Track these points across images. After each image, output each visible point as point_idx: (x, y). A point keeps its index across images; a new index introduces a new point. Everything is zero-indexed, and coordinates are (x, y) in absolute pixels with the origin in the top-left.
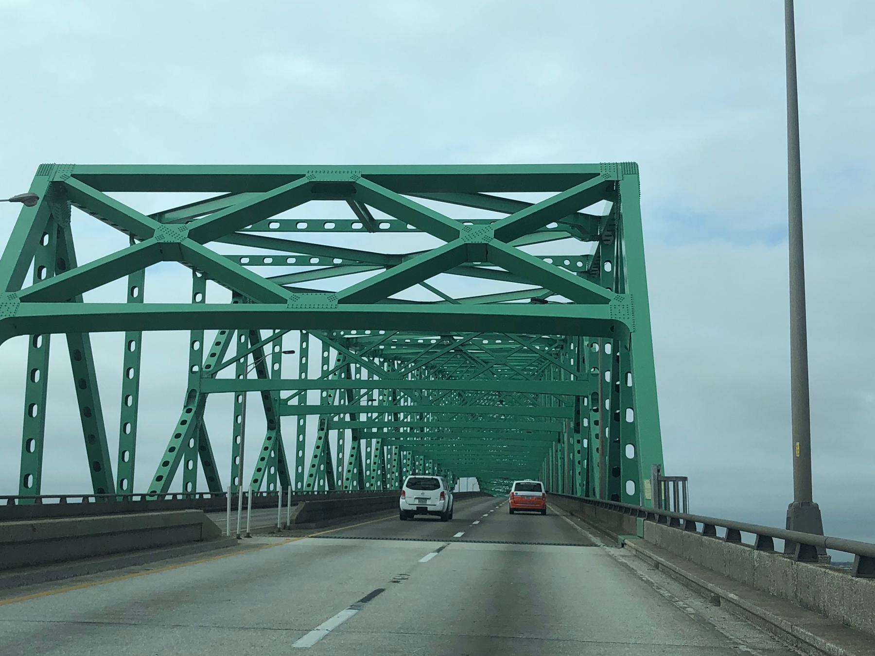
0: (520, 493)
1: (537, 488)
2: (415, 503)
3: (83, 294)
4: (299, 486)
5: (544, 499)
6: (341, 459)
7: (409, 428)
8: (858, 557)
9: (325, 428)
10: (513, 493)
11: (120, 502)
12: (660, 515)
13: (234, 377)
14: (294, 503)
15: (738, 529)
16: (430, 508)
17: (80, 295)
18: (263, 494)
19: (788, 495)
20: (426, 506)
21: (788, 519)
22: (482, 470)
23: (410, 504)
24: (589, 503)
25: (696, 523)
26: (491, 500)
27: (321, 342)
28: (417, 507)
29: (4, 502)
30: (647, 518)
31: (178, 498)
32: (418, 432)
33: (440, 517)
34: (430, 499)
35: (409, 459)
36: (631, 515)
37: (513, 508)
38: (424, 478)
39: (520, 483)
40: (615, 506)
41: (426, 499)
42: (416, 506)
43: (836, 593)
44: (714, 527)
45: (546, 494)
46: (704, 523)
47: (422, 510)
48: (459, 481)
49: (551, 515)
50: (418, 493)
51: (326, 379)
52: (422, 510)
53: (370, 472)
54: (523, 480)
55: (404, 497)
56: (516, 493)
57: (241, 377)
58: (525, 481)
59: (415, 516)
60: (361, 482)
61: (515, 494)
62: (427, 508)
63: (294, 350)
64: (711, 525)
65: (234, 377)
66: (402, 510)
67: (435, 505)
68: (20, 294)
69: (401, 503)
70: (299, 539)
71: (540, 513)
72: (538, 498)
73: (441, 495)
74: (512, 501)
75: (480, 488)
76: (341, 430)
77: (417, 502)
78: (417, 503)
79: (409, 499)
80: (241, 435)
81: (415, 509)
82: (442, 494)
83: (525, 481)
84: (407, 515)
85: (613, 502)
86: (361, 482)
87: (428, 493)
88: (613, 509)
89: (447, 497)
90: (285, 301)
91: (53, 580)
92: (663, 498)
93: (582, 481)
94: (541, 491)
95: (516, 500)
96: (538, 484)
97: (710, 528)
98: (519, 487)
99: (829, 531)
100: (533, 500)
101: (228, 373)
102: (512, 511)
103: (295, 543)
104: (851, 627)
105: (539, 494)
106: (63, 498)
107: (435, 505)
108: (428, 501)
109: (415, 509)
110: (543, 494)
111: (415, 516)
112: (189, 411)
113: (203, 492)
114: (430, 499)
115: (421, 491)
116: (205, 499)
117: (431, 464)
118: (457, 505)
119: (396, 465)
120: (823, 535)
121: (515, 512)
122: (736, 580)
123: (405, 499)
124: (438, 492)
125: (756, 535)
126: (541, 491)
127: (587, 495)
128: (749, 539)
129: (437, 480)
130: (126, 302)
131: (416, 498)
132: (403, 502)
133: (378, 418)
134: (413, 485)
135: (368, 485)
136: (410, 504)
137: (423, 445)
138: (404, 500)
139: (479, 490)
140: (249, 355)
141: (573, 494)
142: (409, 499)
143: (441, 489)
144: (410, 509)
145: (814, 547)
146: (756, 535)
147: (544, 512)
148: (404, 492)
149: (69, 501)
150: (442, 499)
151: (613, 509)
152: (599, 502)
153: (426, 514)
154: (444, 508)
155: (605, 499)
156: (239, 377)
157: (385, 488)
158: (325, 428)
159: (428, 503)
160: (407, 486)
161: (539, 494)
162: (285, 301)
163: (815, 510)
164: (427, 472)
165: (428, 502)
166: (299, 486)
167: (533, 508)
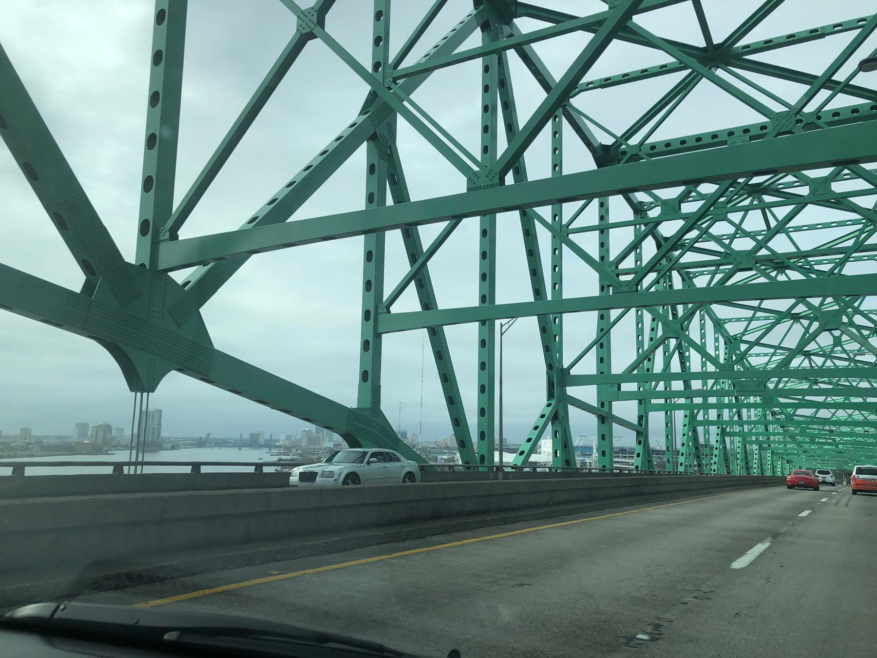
0: (861, 476)
3: (497, 214)
7: (734, 398)
10: (854, 476)
14: (858, 471)
16: (827, 481)
22: (614, 471)
27: (839, 94)
29: (8, 472)
32: (740, 397)
41: (825, 478)
51: (808, 335)
54: (864, 465)
61: (856, 477)
80: (650, 451)
82: (832, 476)
83: (866, 466)
87: (825, 476)
92: (799, 77)
98: (859, 471)
102: (855, 492)
103: (142, 606)
121: (858, 493)
130: (513, 183)
140: (465, 221)
143: (831, 474)
149: (204, 469)
160: (817, 473)
165: (826, 479)
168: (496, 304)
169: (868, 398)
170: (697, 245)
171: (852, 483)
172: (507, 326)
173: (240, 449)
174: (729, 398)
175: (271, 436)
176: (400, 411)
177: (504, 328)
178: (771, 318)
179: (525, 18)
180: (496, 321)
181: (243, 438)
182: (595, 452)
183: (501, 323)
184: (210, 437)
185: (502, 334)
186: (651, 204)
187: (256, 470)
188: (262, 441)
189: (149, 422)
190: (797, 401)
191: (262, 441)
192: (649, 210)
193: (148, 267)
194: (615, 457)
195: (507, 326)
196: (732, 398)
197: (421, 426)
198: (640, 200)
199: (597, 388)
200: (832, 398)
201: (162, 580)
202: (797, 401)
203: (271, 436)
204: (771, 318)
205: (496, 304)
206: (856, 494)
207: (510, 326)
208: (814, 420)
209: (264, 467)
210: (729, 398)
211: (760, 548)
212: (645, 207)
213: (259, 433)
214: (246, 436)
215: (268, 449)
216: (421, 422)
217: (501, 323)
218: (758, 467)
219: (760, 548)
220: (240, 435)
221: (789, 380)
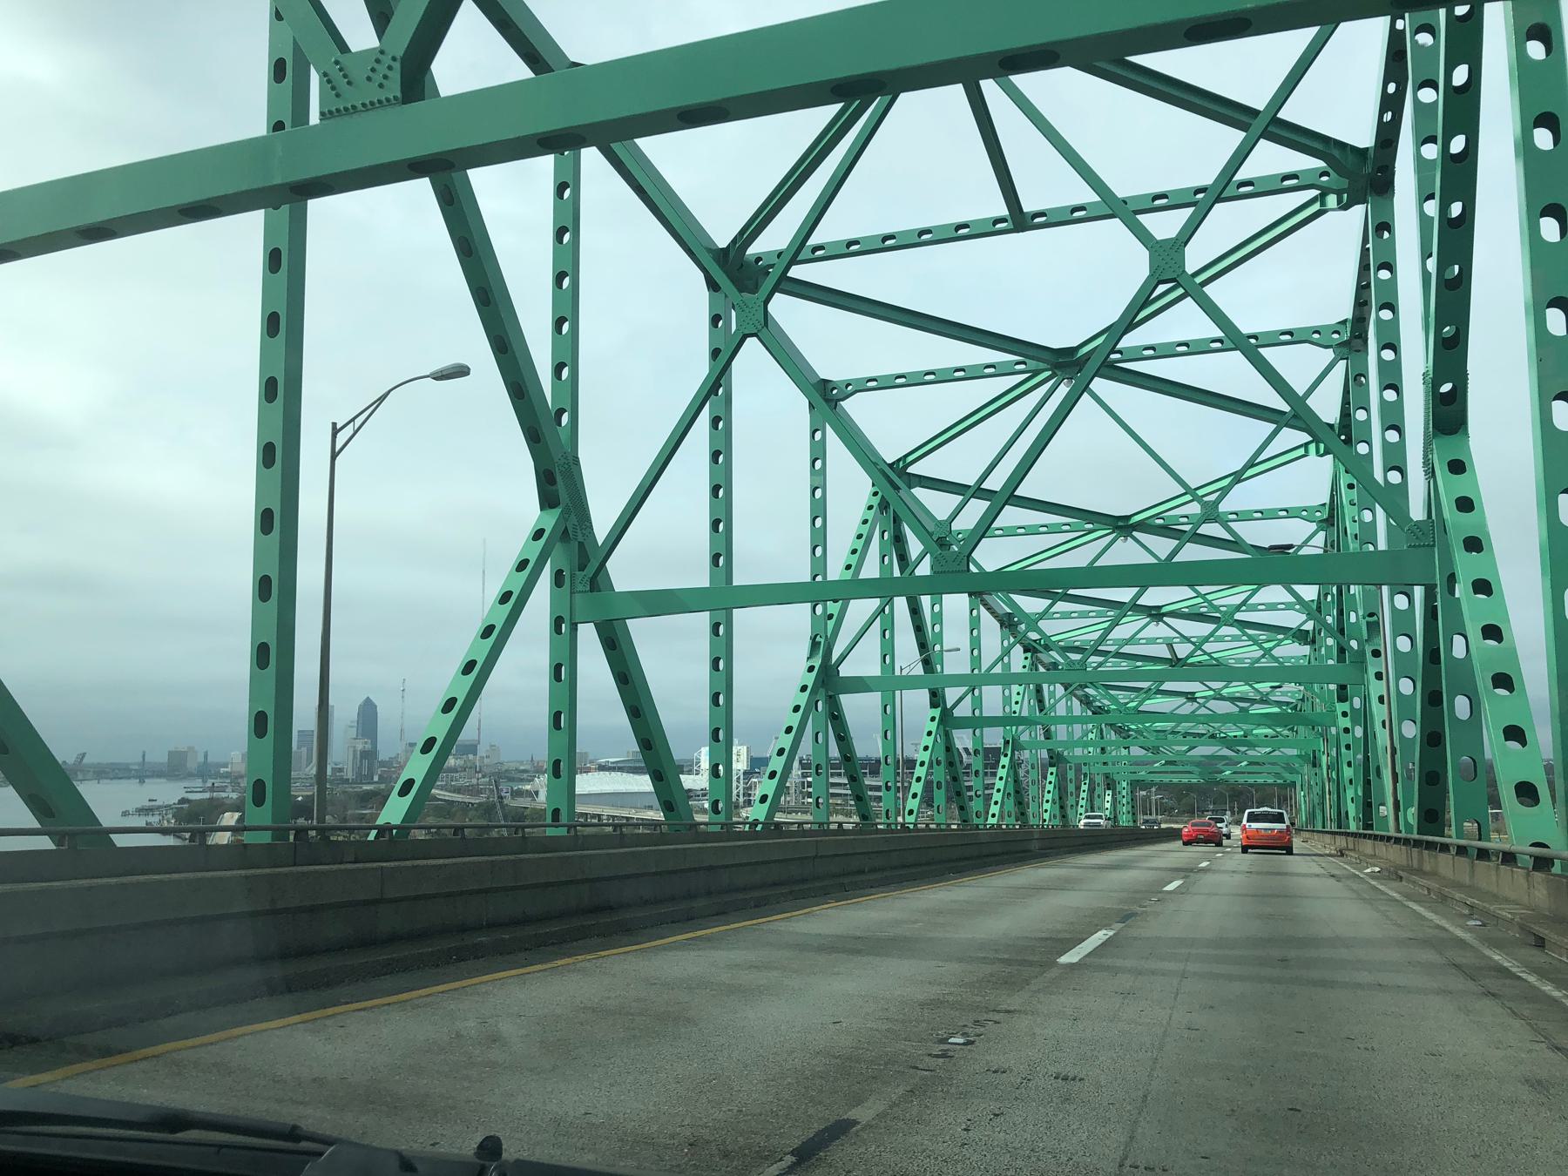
0: (1255, 825)
1: (1279, 818)
13: (808, 579)
17: (303, 202)
21: (358, 714)
30: (1502, 862)
36: (1426, 849)
40: (1370, 835)
43: (995, 765)
48: (1283, 854)
57: (819, 578)
58: (1261, 809)
65: (808, 579)
71: (1284, 852)
72: (1280, 831)
85: (1366, 832)
93: (1357, 813)
94: (1284, 823)
101: (861, 609)
110: (1287, 826)
126: (1284, 823)
127: (1368, 826)
133: (1308, 684)
141: (1324, 827)
145: (1465, 847)
147: (1290, 852)
155: (1412, 833)
156: (814, 578)
157: (1025, 824)
168: (734, 584)
170: (796, 272)
172: (349, 430)
173: (142, 782)
175: (206, 756)
176: (403, 697)
177: (342, 438)
178: (1091, 614)
179: (918, 488)
181: (209, 760)
182: (797, 767)
183: (334, 424)
184: (85, 761)
185: (334, 456)
186: (847, 387)
188: (192, 765)
190: (1071, 592)
191: (192, 765)
192: (843, 400)
194: (832, 775)
195: (349, 430)
197: (479, 729)
198: (822, 377)
199: (882, 697)
201: (34, 1040)
202: (1071, 592)
203: (206, 756)
204: (1091, 614)
205: (734, 584)
207: (355, 432)
211: (1101, 936)
212: (835, 392)
213: (186, 749)
214: (159, 756)
215: (200, 780)
216: (480, 721)
217: (334, 424)
218: (1128, 803)
219: (1101, 936)
220: (141, 754)
221: (1106, 661)
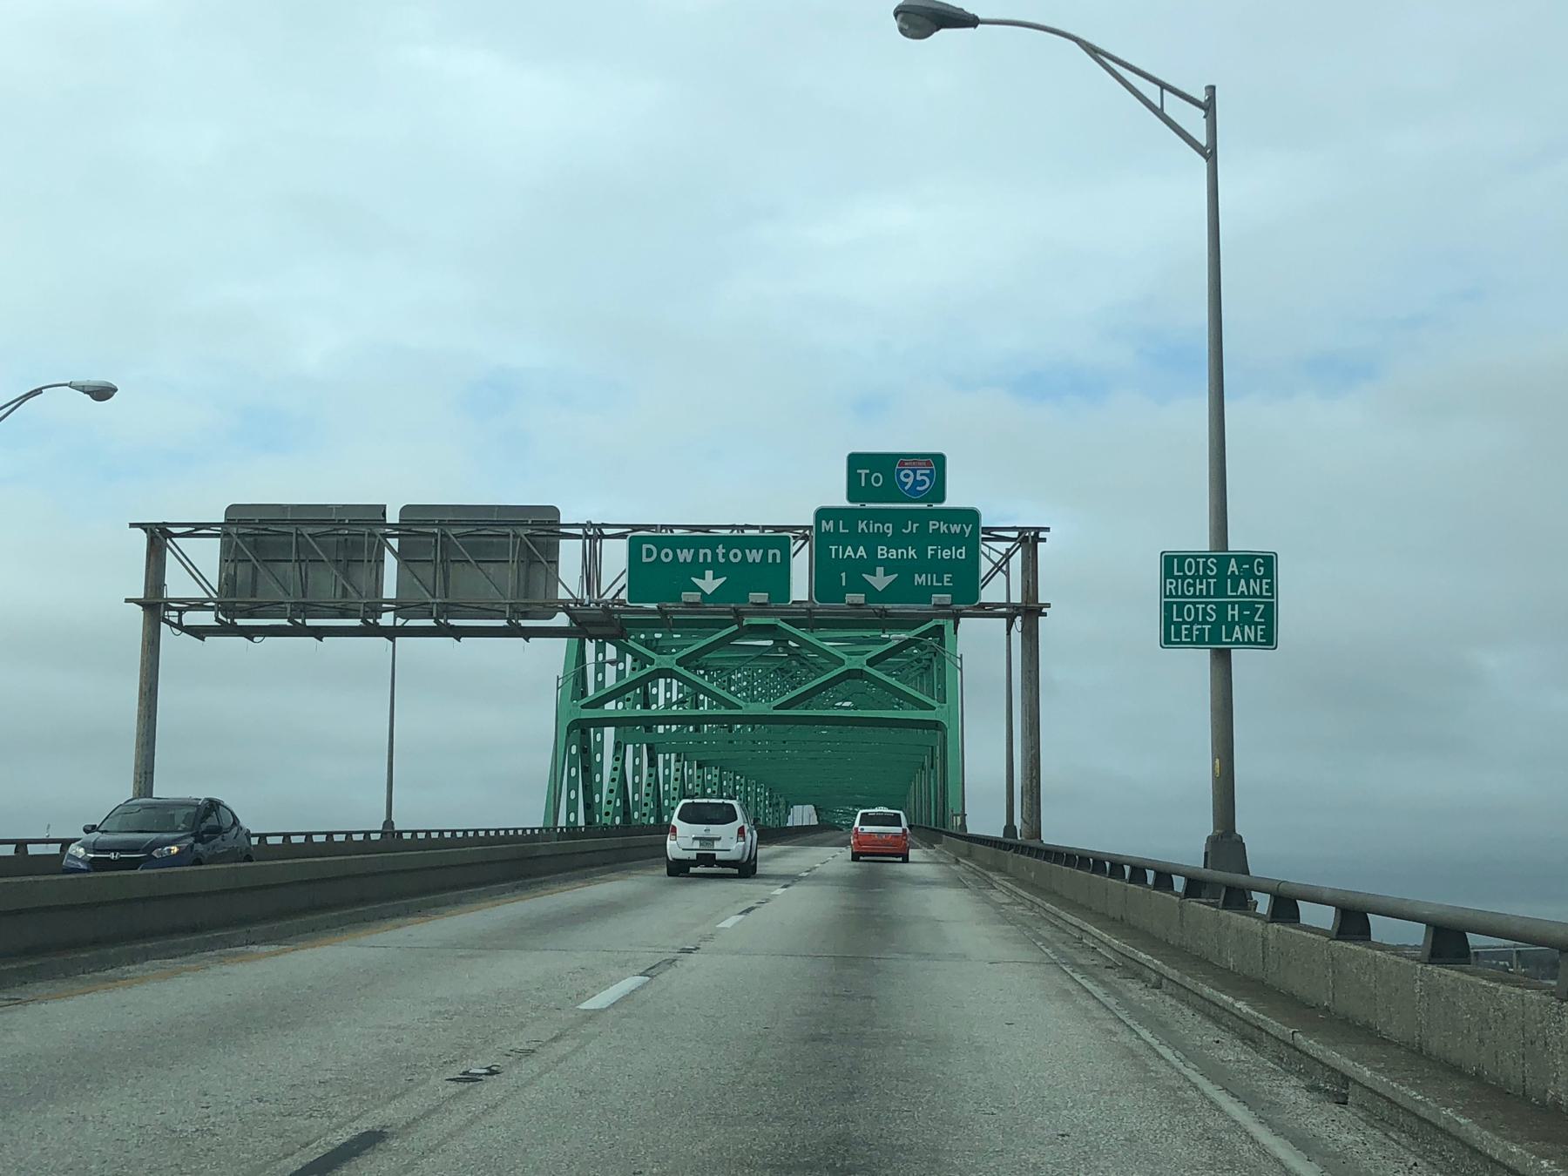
0: (868, 829)
1: (895, 821)
2: (694, 848)
4: (572, 818)
5: (904, 838)
6: (638, 784)
8: (1431, 929)
9: (682, 759)
10: (857, 828)
11: (448, 838)
12: (1227, 887)
15: (1364, 910)
16: (719, 856)
18: (457, 833)
19: (1206, 826)
20: (713, 852)
23: (683, 849)
24: (986, 845)
25: (1173, 876)
26: (841, 835)
28: (698, 854)
29: (9, 850)
31: (404, 838)
33: (736, 871)
34: (719, 839)
35: (716, 776)
37: (857, 852)
38: (708, 804)
39: (867, 813)
41: (713, 840)
42: (695, 852)
44: (1171, 877)
45: (908, 831)
46: (1429, 924)
47: (706, 859)
49: (927, 883)
50: (700, 829)
52: (706, 859)
53: (669, 802)
55: (674, 837)
56: (862, 829)
58: (876, 810)
59: (692, 870)
60: (626, 813)
62: (714, 855)
63: (115, 383)
64: (1141, 869)
66: (671, 859)
67: (729, 850)
68: (585, 701)
69: (668, 847)
70: (285, 952)
72: (896, 836)
73: (739, 833)
74: (856, 840)
75: (818, 820)
76: (637, 745)
77: (697, 845)
78: (698, 848)
79: (683, 840)
81: (695, 858)
82: (741, 831)
83: (876, 810)
84: (679, 869)
86: (626, 813)
87: (715, 830)
88: (1019, 852)
89: (748, 835)
90: (741, 708)
91: (420, 911)
94: (901, 826)
95: (863, 839)
96: (895, 814)
97: (1285, 907)
98: (866, 820)
99: (1256, 869)
100: (888, 839)
104: (1431, 1057)
105: (898, 830)
106: (21, 844)
107: (729, 850)
108: (715, 843)
109: (695, 858)
110: (904, 830)
111: (692, 870)
112: (617, 759)
113: (289, 831)
114: (719, 839)
115: (705, 826)
116: (316, 843)
117: (743, 787)
118: (763, 851)
119: (716, 790)
120: (1248, 873)
121: (861, 858)
122: (1385, 1042)
123: (676, 840)
124: (732, 828)
125: (1334, 908)
126: (901, 826)
128: (1319, 916)
129: (732, 805)
131: (695, 839)
132: (671, 845)
134: (690, 815)
135: (636, 815)
136: (683, 849)
137: (700, 742)
138: (675, 842)
139: (817, 823)
142: (683, 840)
144: (686, 857)
146: (1334, 908)
148: (674, 828)
149: (33, 850)
150: (742, 839)
151: (1019, 852)
152: (1024, 847)
153: (712, 866)
154: (743, 857)
158: (682, 759)
159: (715, 848)
160: (679, 818)
161: (898, 830)
162: (741, 708)
163: (1239, 844)
164: (709, 791)
165: (717, 845)
166: (572, 818)
167: (893, 852)
169: (358, 625)
171: (852, 842)
174: (666, 681)
180: (644, 545)
187: (364, 837)
189: (940, 774)
193: (865, 557)
196: (671, 681)
200: (991, 576)
206: (858, 860)
208: (844, 700)
209: (267, 838)
210: (666, 681)
